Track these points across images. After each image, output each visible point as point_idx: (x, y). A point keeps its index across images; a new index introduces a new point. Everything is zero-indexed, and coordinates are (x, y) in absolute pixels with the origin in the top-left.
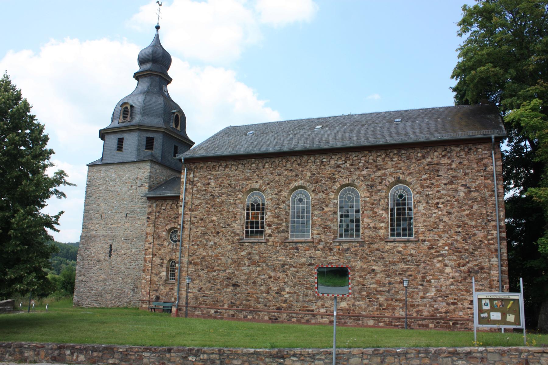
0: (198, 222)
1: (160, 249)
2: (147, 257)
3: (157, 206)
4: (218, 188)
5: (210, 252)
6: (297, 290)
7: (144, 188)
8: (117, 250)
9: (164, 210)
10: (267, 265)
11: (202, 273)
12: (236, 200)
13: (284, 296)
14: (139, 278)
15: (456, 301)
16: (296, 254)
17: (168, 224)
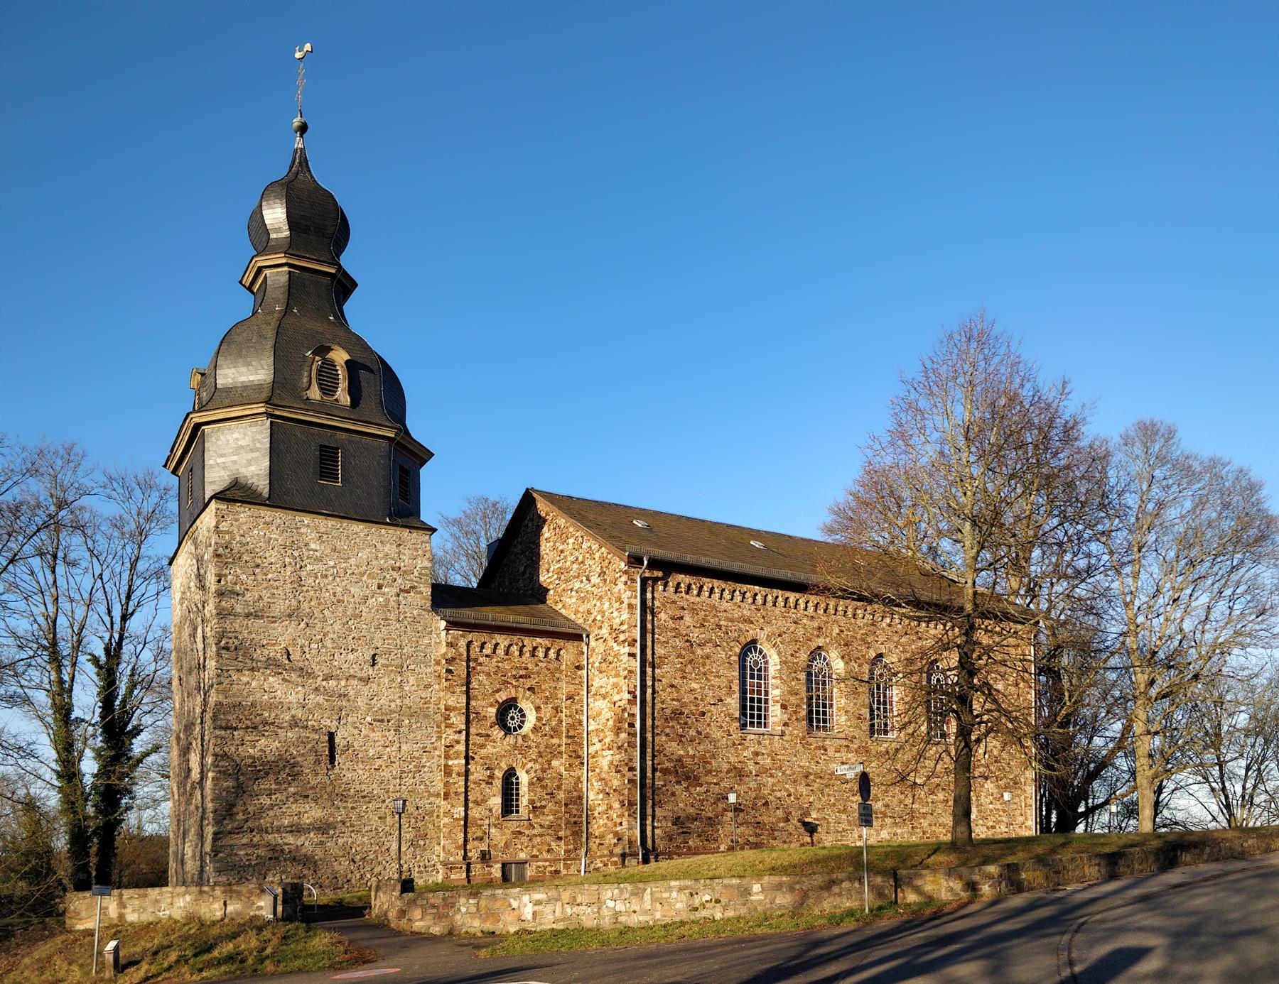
2: (450, 763)
10: (783, 774)
16: (822, 757)
17: (498, 690)
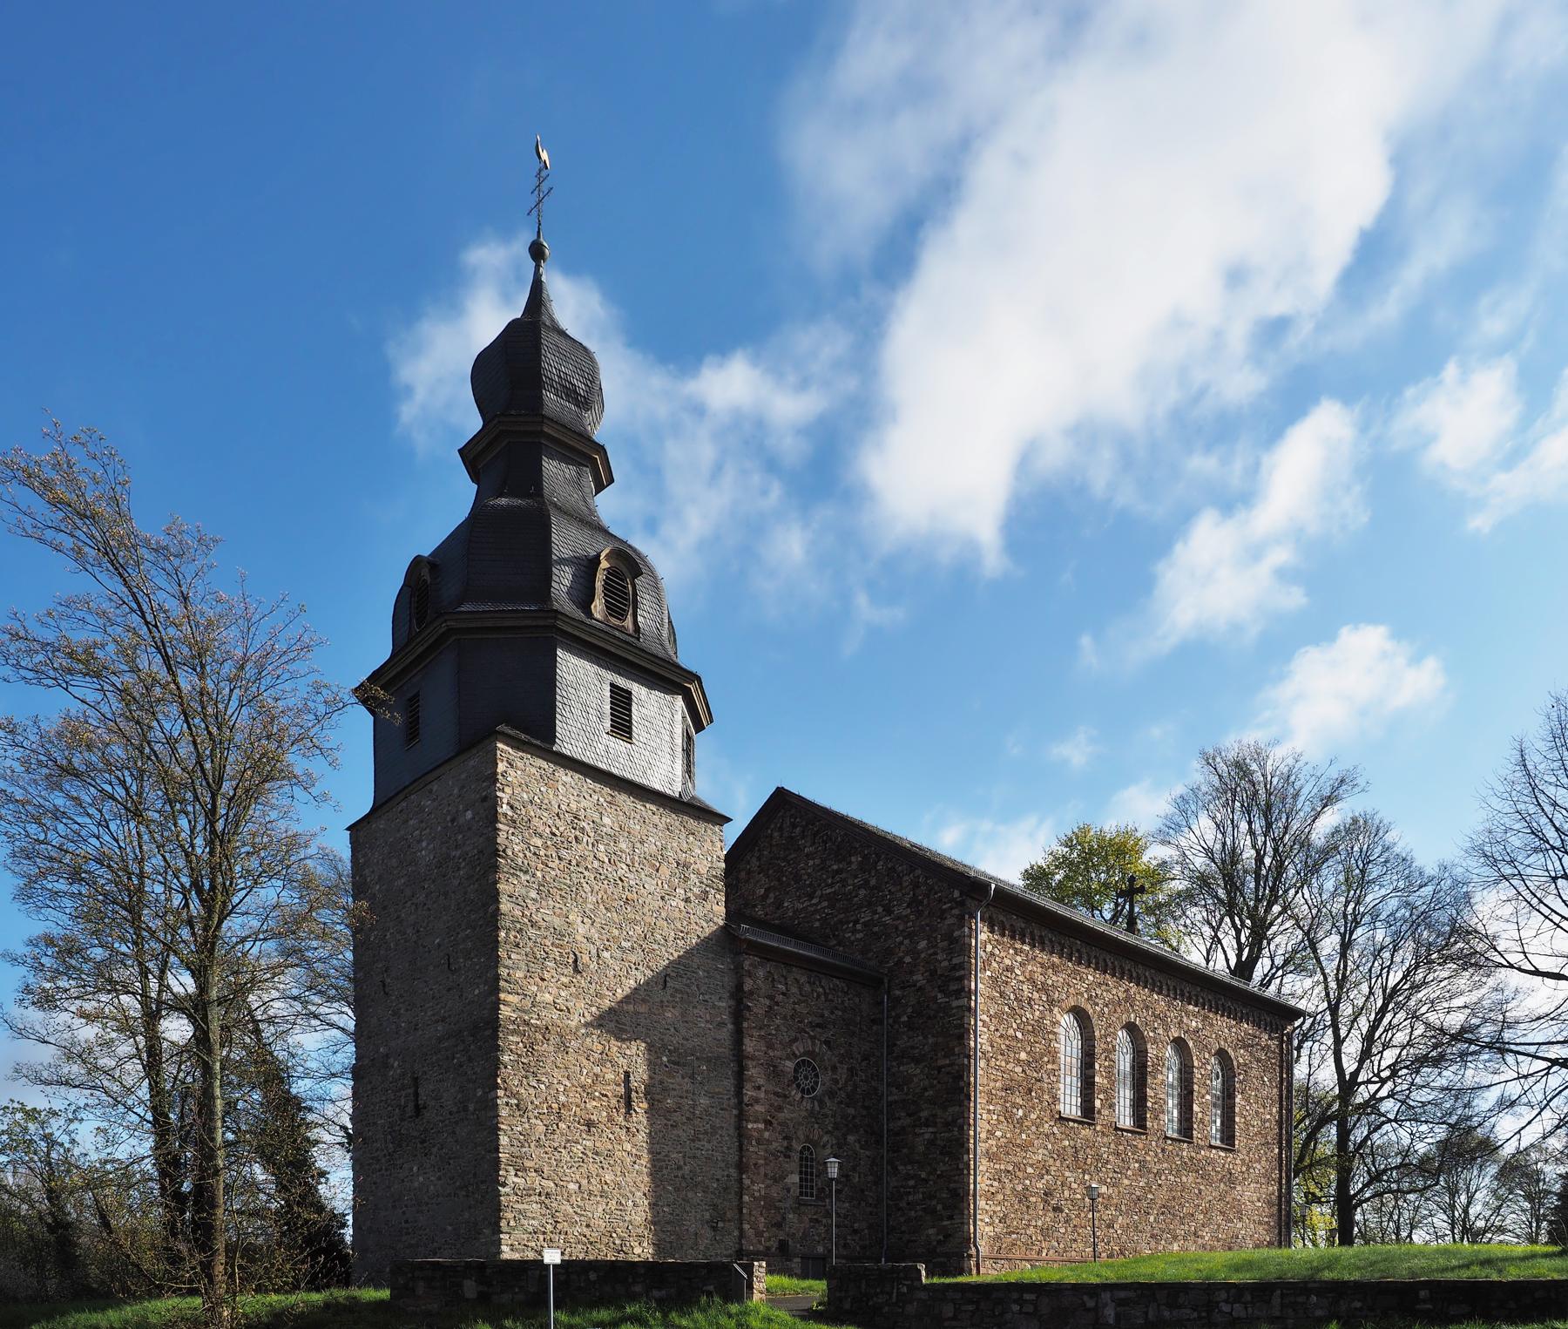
1: (780, 1109)
17: (796, 1040)
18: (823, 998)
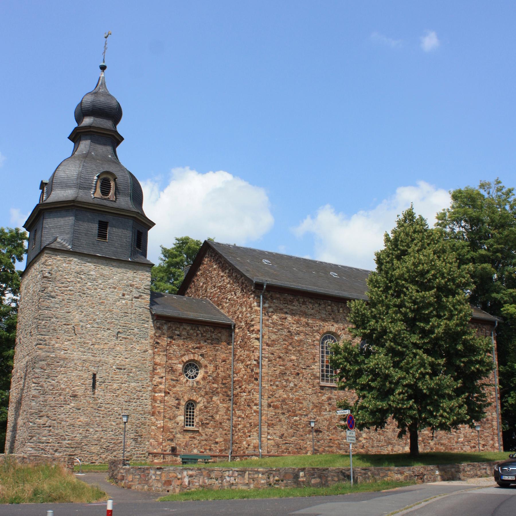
0: (275, 360)
1: (174, 386)
2: (156, 395)
3: (169, 328)
4: (295, 325)
5: (290, 394)
6: (372, 436)
7: (143, 301)
8: (104, 382)
9: (178, 335)
11: (282, 417)
12: (314, 341)
13: (361, 441)
14: (144, 424)
15: (475, 445)
17: (184, 355)
18: (200, 335)
